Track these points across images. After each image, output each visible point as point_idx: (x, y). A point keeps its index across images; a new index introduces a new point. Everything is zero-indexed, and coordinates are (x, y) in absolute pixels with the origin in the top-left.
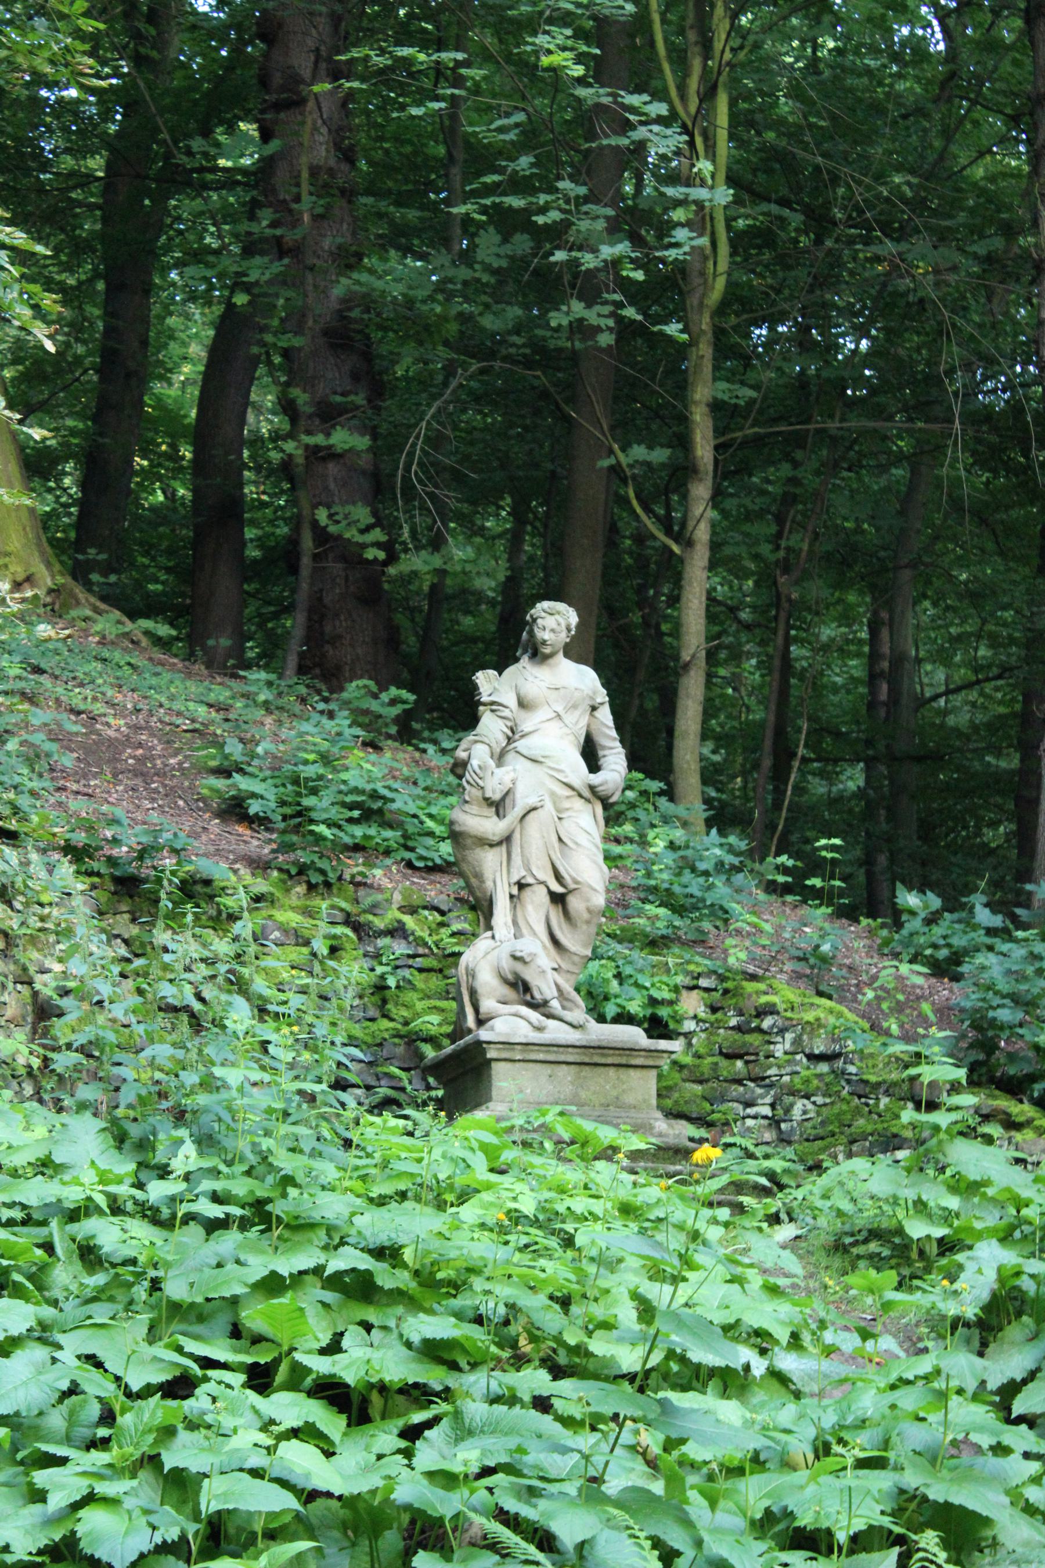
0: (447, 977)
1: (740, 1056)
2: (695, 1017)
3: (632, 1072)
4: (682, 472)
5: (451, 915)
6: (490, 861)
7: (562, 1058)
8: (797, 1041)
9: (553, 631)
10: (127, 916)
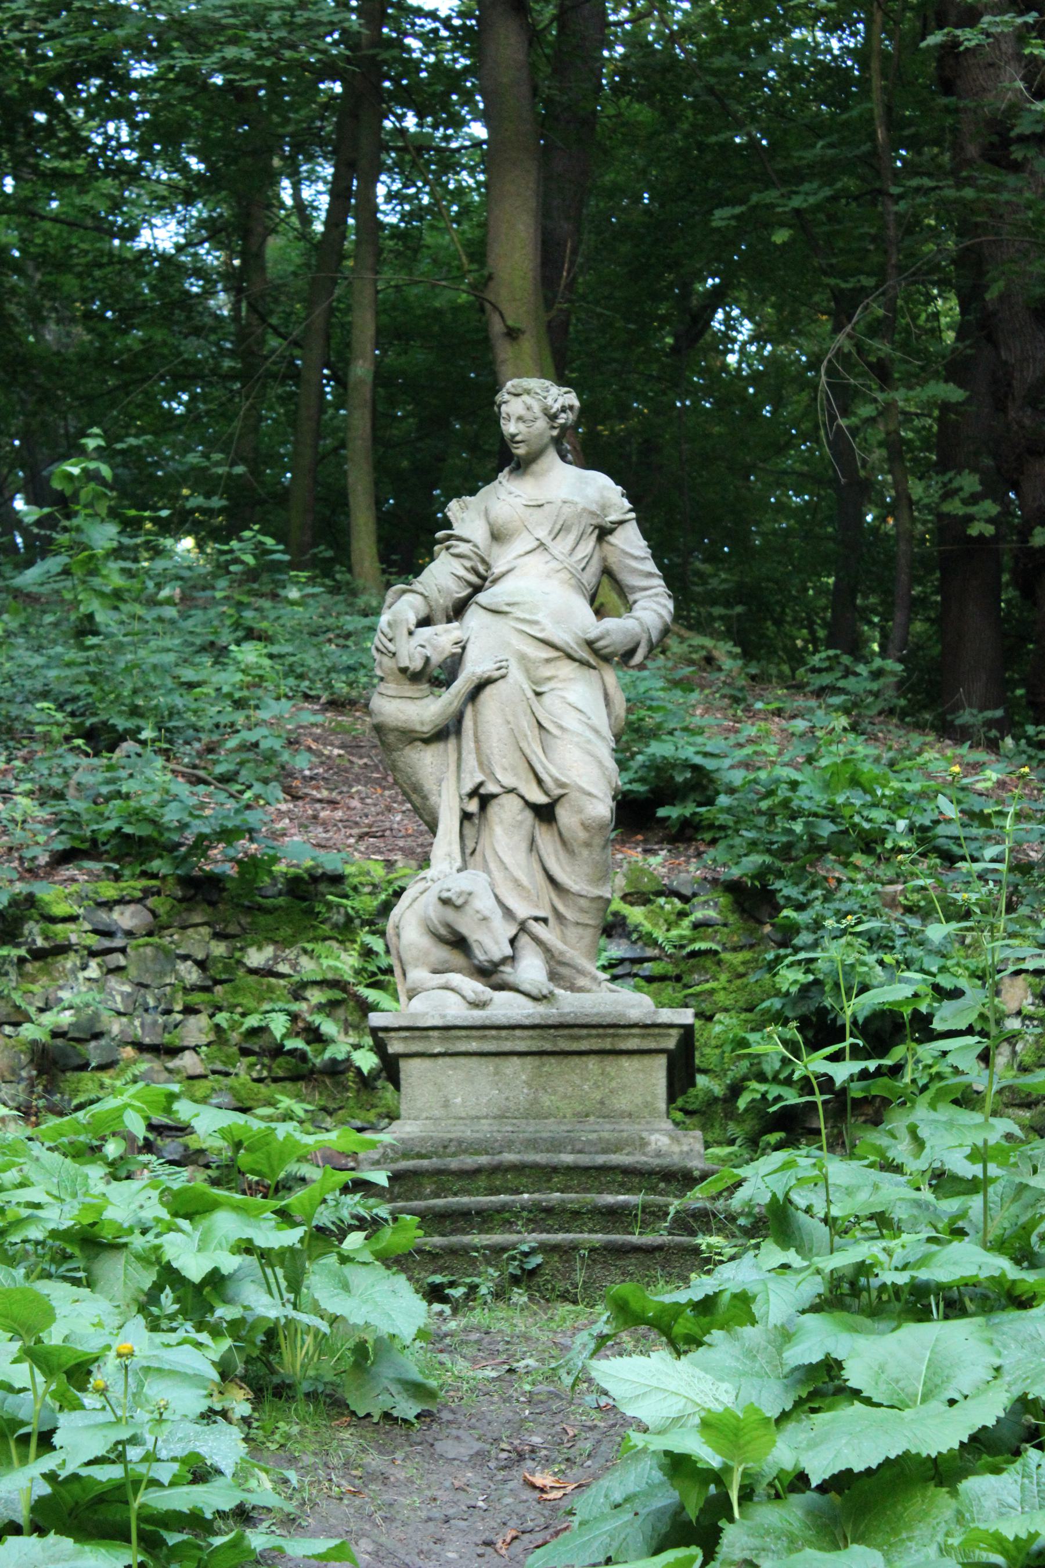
0: (687, 986)
2: (1019, 1013)
3: (625, 1062)
5: (695, 900)
6: (428, 764)
7: (507, 1046)
9: (520, 419)
10: (205, 931)
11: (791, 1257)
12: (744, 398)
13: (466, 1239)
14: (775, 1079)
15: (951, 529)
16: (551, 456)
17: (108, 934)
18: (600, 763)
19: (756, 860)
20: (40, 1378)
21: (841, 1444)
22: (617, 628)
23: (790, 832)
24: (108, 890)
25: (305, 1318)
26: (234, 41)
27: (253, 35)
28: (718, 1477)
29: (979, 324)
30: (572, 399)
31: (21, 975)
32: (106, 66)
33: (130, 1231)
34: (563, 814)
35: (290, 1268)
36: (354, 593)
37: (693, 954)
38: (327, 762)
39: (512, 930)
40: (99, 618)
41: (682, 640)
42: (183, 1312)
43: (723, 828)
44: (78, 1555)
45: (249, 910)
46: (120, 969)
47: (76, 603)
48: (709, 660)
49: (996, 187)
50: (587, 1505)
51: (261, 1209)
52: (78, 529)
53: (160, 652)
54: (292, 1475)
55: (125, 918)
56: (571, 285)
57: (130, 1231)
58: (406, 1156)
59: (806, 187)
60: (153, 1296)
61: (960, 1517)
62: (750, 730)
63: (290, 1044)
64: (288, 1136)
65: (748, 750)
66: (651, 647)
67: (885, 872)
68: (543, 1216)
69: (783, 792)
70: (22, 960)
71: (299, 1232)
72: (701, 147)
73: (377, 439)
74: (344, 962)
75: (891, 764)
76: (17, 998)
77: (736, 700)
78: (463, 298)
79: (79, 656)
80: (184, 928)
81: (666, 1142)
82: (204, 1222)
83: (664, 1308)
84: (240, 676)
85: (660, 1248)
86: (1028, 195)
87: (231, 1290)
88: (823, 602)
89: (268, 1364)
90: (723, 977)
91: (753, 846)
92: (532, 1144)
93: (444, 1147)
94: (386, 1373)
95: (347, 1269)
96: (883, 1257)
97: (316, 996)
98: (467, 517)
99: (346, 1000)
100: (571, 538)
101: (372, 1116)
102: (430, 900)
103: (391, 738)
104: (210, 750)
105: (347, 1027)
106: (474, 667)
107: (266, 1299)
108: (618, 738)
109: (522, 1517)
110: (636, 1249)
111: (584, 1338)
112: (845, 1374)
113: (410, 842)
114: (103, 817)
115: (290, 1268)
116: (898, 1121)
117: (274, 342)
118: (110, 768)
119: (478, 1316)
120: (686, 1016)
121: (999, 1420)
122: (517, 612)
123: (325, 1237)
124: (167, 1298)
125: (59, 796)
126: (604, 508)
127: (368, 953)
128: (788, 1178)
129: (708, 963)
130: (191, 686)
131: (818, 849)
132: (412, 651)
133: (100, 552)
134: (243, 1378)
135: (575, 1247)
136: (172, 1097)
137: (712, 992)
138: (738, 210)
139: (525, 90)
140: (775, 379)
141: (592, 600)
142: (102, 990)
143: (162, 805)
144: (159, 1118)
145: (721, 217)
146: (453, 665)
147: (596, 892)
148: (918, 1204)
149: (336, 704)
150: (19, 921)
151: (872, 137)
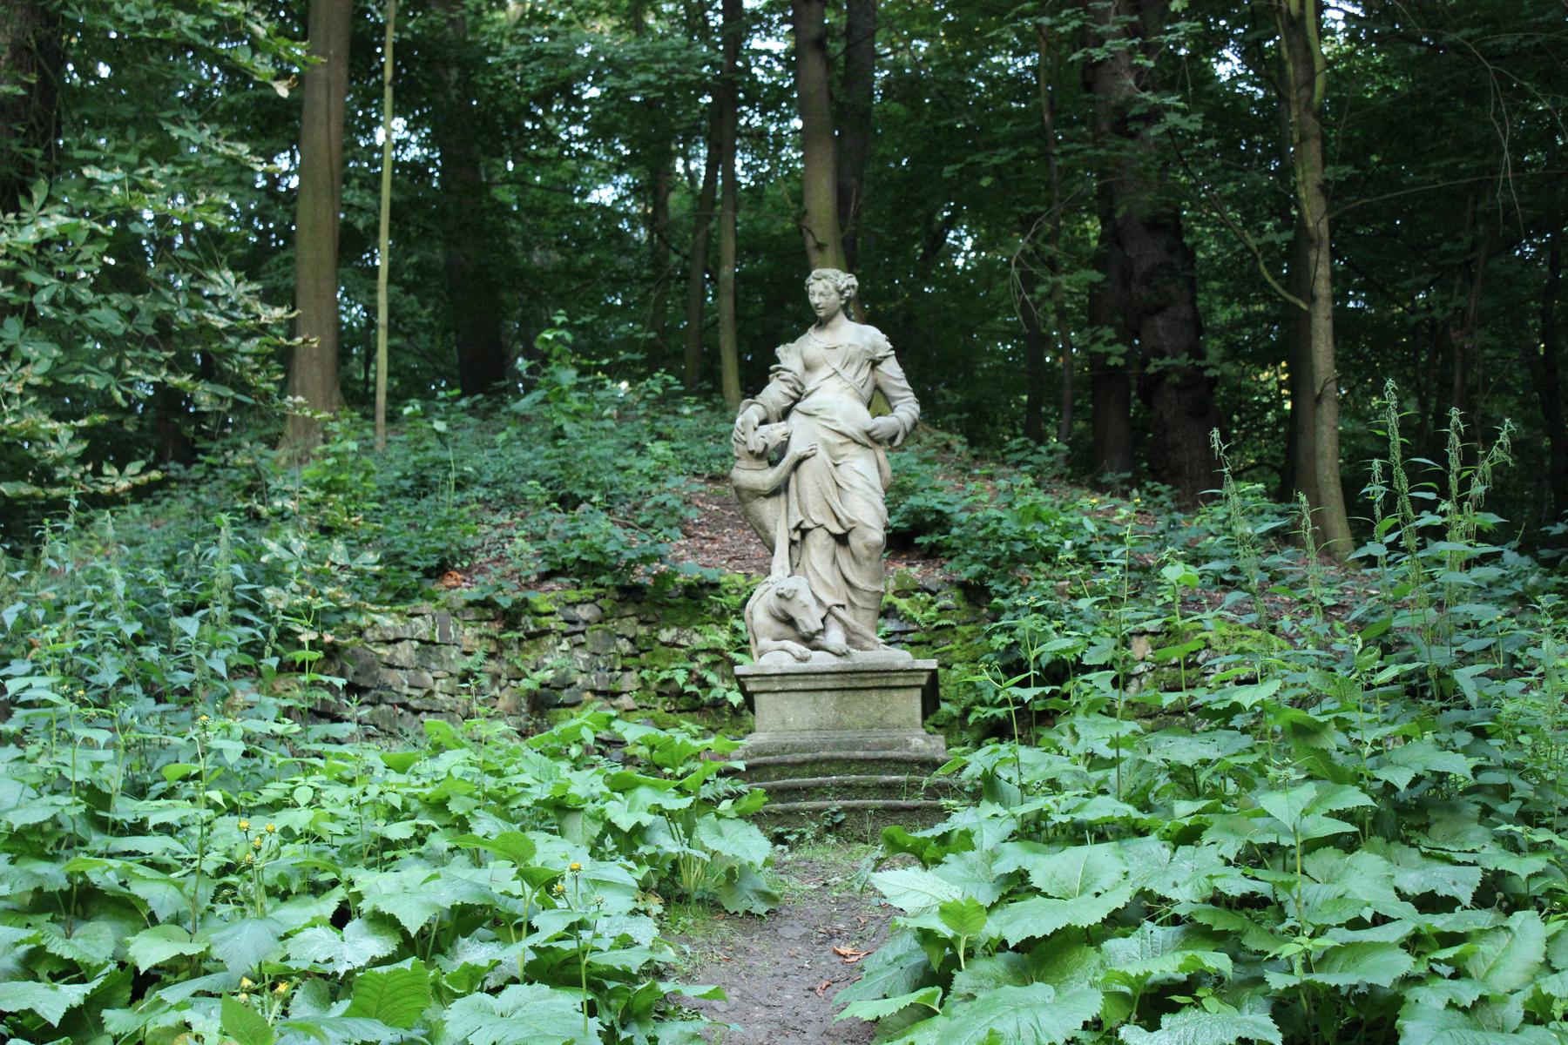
3: (895, 693)
4: (1297, 251)
6: (768, 510)
7: (821, 685)
10: (634, 619)
11: (997, 809)
12: (968, 285)
13: (797, 805)
14: (992, 705)
15: (1097, 361)
16: (841, 317)
17: (574, 622)
18: (876, 508)
19: (977, 567)
20: (528, 889)
21: (1028, 921)
22: (885, 423)
23: (997, 550)
24: (573, 596)
25: (695, 852)
26: (644, 70)
27: (656, 67)
28: (951, 943)
29: (1112, 235)
30: (854, 281)
31: (521, 648)
32: (565, 89)
33: (586, 800)
34: (853, 539)
35: (685, 822)
36: (725, 410)
37: (939, 628)
38: (708, 514)
39: (823, 613)
40: (566, 428)
41: (930, 435)
42: (620, 850)
43: (956, 549)
44: (551, 996)
45: (660, 606)
46: (581, 644)
47: (551, 420)
48: (948, 447)
49: (1119, 148)
50: (870, 964)
51: (666, 787)
52: (552, 373)
53: (604, 448)
54: (687, 948)
55: (584, 612)
56: (857, 215)
57: (586, 800)
58: (759, 754)
59: (1001, 151)
60: (600, 840)
61: (1102, 965)
62: (972, 486)
63: (688, 689)
64: (683, 742)
65: (970, 499)
66: (907, 435)
67: (1057, 573)
68: (845, 790)
69: (993, 524)
70: (521, 640)
71: (690, 800)
72: (936, 129)
73: (737, 317)
74: (721, 637)
75: (1061, 507)
76: (518, 663)
77: (964, 470)
78: (789, 226)
79: (554, 452)
80: (621, 618)
81: (922, 742)
82: (631, 795)
83: (918, 841)
84: (653, 462)
85: (918, 808)
86: (1140, 153)
87: (648, 836)
88: (1021, 410)
89: (673, 882)
90: (958, 642)
91: (975, 559)
92: (837, 746)
93: (783, 749)
94: (747, 886)
95: (721, 822)
96: (1053, 806)
97: (704, 659)
98: (789, 356)
99: (720, 660)
100: (855, 367)
101: (740, 732)
102: (771, 594)
103: (745, 495)
104: (636, 508)
105: (723, 677)
106: (795, 450)
107: (671, 841)
108: (886, 491)
109: (832, 974)
110: (904, 809)
111: (867, 862)
112: (1031, 879)
113: (761, 562)
114: (569, 550)
115: (685, 822)
116: (1063, 723)
117: (675, 258)
118: (573, 520)
119: (805, 852)
120: (933, 664)
121: (1127, 905)
122: (822, 415)
123: (709, 803)
124: (609, 841)
125: (542, 538)
126: (875, 348)
127: (735, 631)
128: (994, 759)
129: (949, 633)
130: (623, 469)
131: (1015, 560)
132: (758, 439)
133: (565, 387)
134: (657, 890)
135: (865, 809)
136: (611, 719)
137: (951, 651)
138: (959, 166)
139: (825, 96)
140: (985, 272)
141: (869, 406)
142: (570, 657)
143: (606, 541)
144: (604, 734)
145: (948, 171)
146: (783, 448)
147: (875, 588)
148: (1075, 773)
149: (714, 479)
150: (518, 616)
151: (1042, 118)
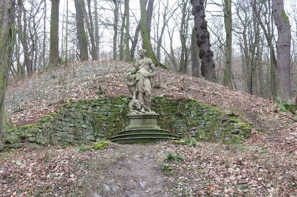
1: (200, 116)
3: (152, 119)
8: (208, 113)
106: (137, 79)
